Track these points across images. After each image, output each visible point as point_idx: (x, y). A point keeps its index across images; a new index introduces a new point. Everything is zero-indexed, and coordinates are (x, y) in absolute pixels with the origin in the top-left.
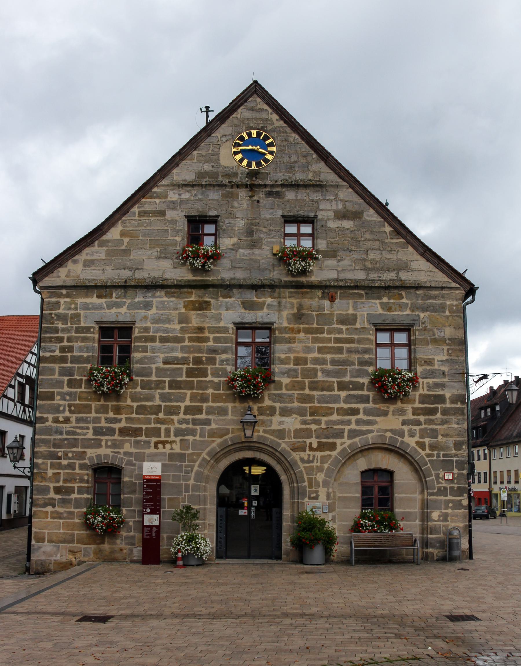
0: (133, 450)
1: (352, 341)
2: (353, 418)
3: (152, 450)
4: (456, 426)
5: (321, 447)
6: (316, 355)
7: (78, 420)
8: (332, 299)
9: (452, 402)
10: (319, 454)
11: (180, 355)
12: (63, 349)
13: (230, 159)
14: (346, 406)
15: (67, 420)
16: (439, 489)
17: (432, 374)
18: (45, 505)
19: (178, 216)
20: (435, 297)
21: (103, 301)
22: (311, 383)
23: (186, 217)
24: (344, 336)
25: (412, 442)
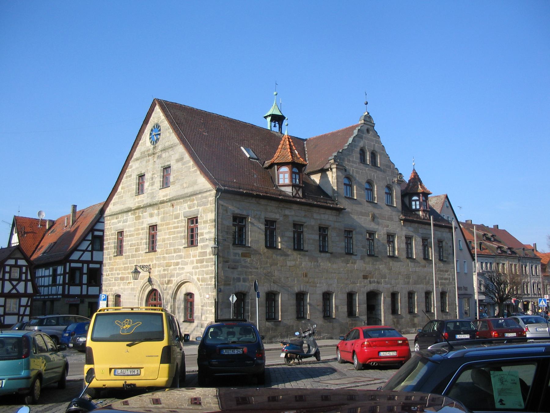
0: (123, 287)
2: (177, 267)
24: (176, 225)
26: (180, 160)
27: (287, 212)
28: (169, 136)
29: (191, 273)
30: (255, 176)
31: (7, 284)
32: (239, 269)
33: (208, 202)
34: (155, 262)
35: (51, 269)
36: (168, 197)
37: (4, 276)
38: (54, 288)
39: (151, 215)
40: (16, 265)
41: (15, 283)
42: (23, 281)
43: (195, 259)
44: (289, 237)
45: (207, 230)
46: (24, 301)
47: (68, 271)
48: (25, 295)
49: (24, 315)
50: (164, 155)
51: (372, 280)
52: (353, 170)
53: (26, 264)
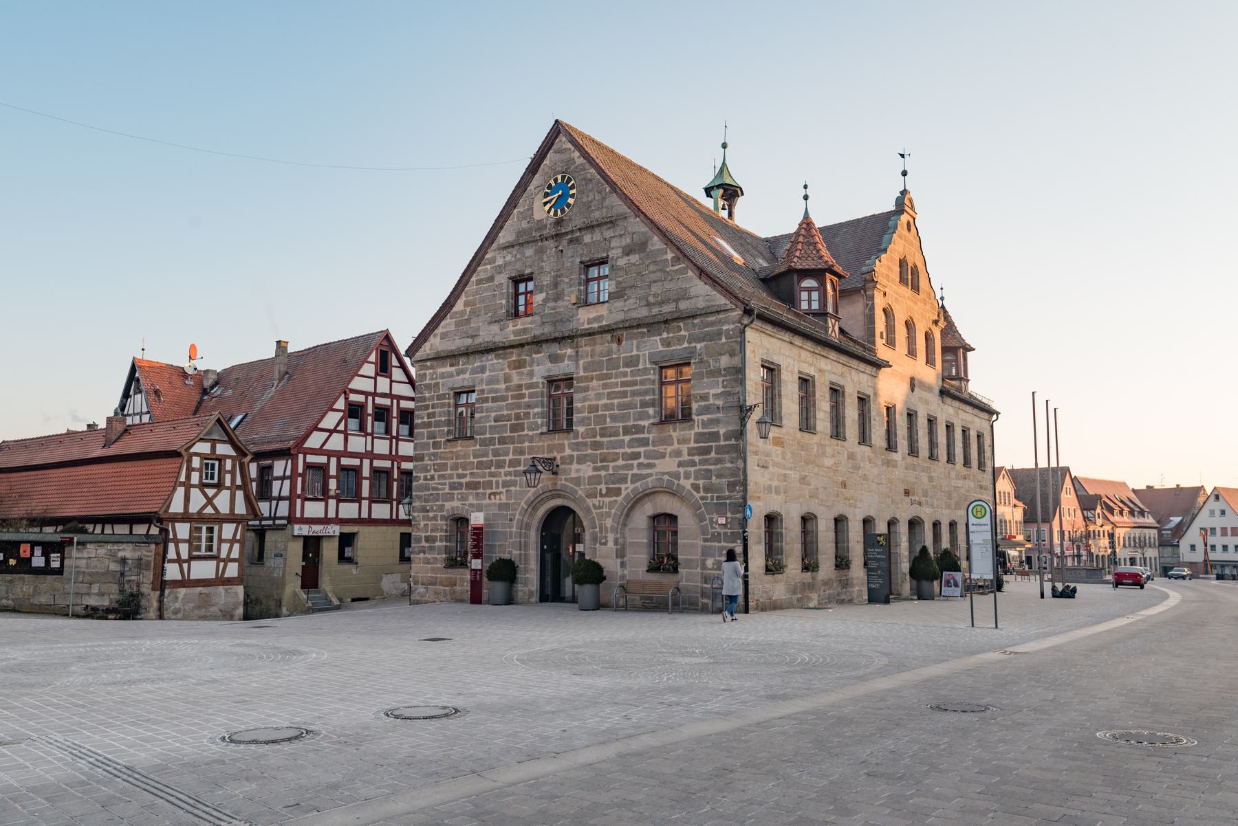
0: (475, 502)
1: (634, 383)
2: (635, 462)
3: (487, 501)
4: (729, 465)
5: (610, 492)
6: (605, 401)
7: (440, 477)
8: (619, 341)
9: (726, 439)
10: (607, 500)
11: (505, 413)
12: (429, 416)
13: (541, 211)
14: (629, 451)
15: (432, 478)
16: (713, 534)
17: (705, 410)
18: (420, 552)
19: (502, 279)
20: (712, 324)
21: (453, 369)
22: (601, 429)
23: (511, 278)
24: (629, 379)
25: (687, 484)
29: (677, 476)
31: (195, 493)
36: (604, 323)
37: (188, 477)
40: (212, 456)
41: (210, 492)
42: (228, 488)
43: (684, 448)
46: (228, 530)
47: (300, 470)
48: (232, 518)
49: (229, 560)
50: (587, 238)
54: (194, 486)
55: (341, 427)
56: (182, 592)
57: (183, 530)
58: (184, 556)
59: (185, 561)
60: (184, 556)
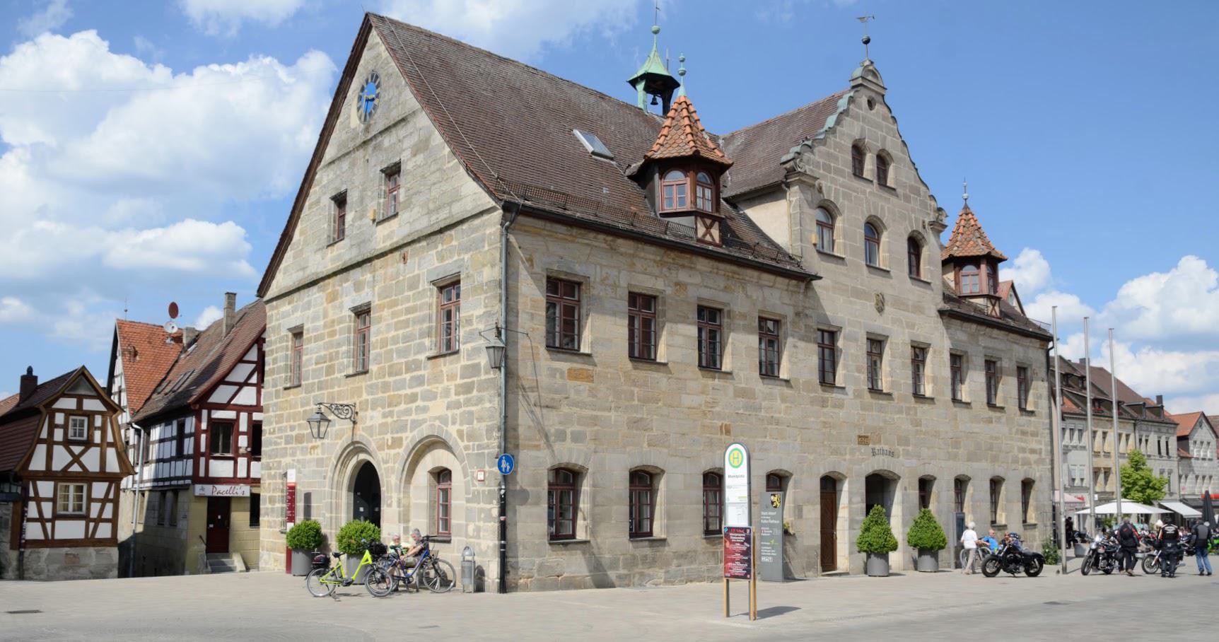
2: (413, 405)
24: (411, 304)
26: (422, 147)
27: (683, 276)
28: (401, 96)
29: (444, 420)
30: (605, 191)
31: (59, 451)
32: (565, 409)
33: (483, 241)
34: (365, 396)
35: (175, 423)
37: (51, 433)
38: (179, 464)
39: (358, 287)
40: (79, 411)
41: (77, 450)
42: (97, 445)
43: (452, 385)
44: (689, 337)
45: (481, 311)
49: (99, 520)
51: (877, 447)
52: (837, 191)
53: (103, 409)
54: (58, 443)
55: (254, 380)
56: (46, 552)
57: (45, 488)
58: (48, 513)
59: (48, 520)
60: (48, 513)
